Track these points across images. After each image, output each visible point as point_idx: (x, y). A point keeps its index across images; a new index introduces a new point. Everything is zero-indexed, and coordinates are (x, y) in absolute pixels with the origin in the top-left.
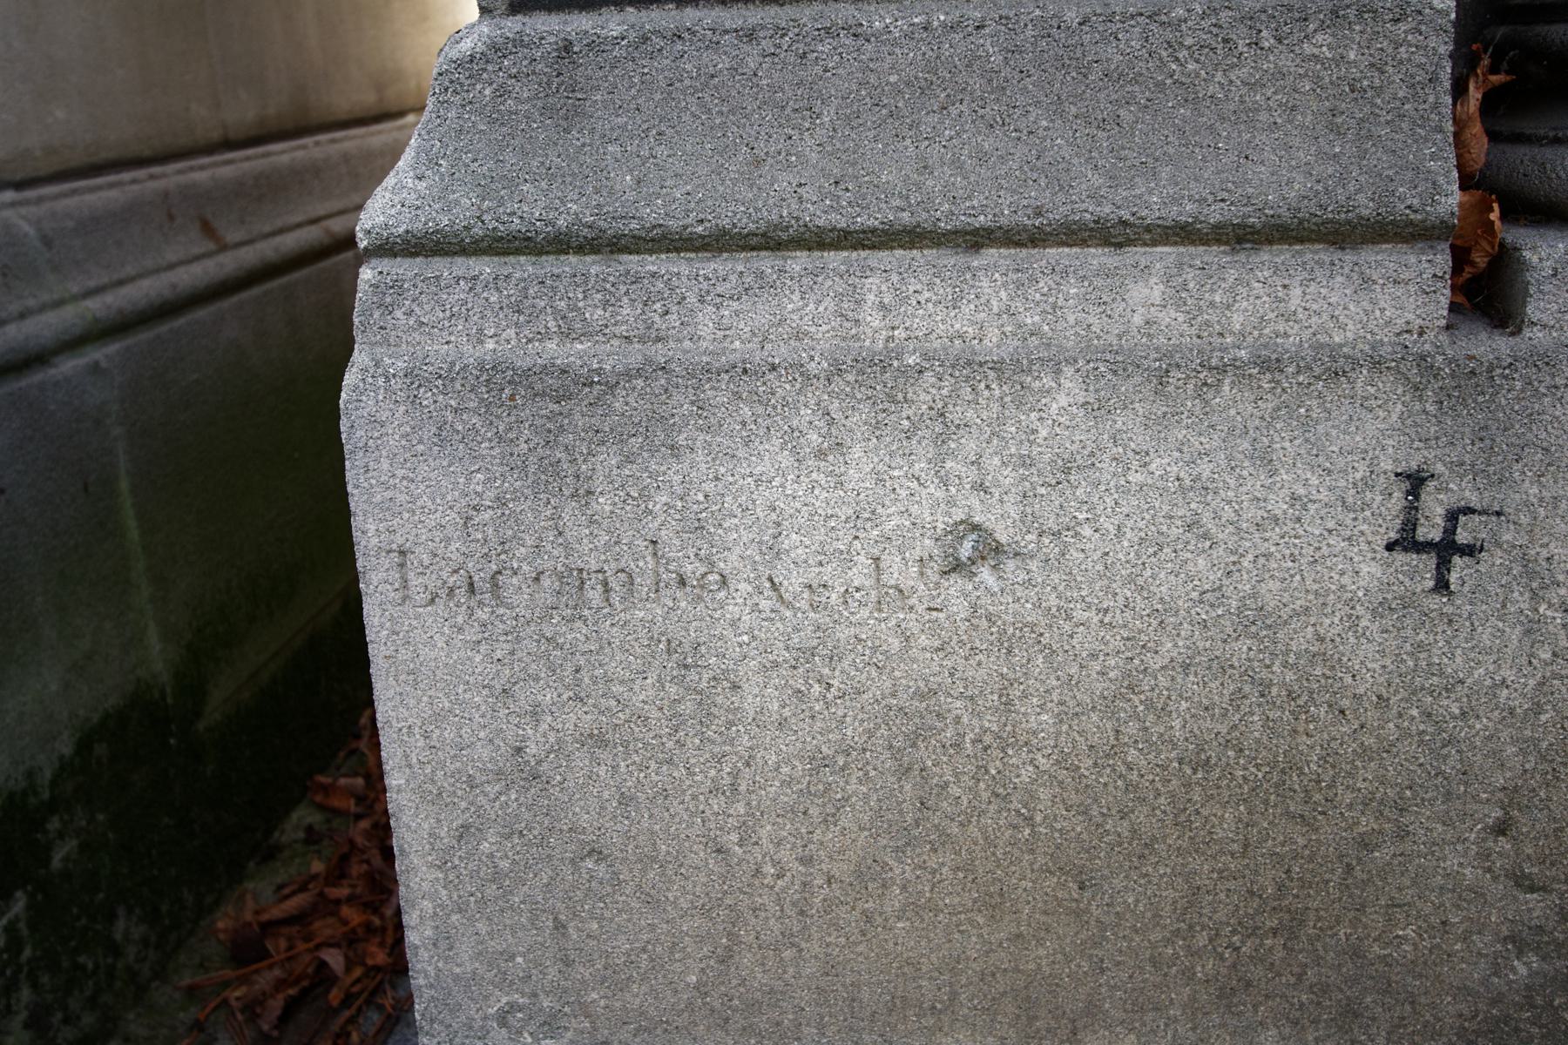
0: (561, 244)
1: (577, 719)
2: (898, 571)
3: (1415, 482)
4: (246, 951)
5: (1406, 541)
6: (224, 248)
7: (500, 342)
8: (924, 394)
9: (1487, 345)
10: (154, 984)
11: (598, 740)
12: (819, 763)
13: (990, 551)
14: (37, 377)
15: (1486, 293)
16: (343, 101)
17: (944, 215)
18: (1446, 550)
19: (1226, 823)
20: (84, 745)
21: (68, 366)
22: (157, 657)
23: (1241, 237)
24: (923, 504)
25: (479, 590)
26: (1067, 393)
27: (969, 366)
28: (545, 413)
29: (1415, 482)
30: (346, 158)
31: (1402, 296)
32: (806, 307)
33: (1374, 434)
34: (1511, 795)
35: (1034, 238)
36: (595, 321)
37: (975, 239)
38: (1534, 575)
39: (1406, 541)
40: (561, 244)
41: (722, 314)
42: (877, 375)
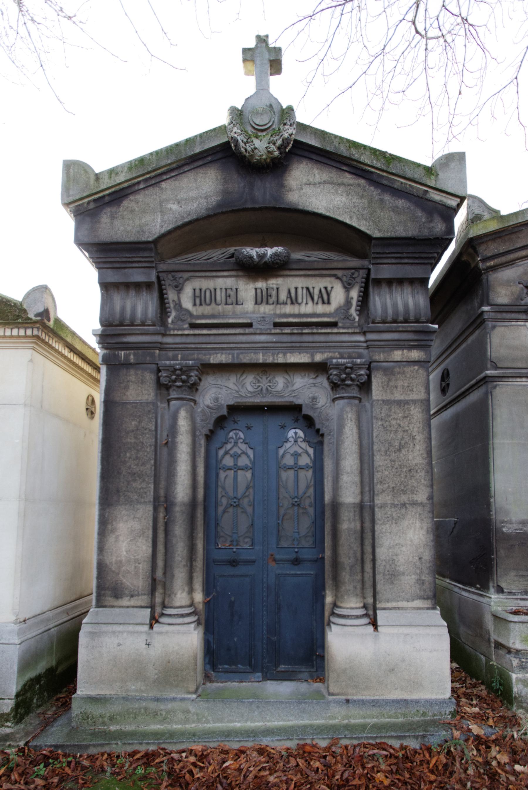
0: (95, 623)
1: (92, 657)
2: (115, 646)
3: (147, 640)
4: (57, 700)
5: (146, 644)
6: (69, 615)
7: (91, 630)
8: (117, 634)
9: (151, 631)
10: (137, 520)
11: (93, 659)
12: (109, 660)
13: (121, 645)
14: (50, 631)
15: (151, 627)
16: (86, 594)
17: (119, 622)
18: (149, 645)
19: (136, 665)
20: (46, 671)
21: (52, 630)
22: (54, 663)
23: (137, 624)
24: (116, 641)
25: (87, 647)
26: (125, 634)
27: (119, 632)
28: (93, 635)
29: (147, 640)
30: (86, 602)
31: (146, 628)
32: (110, 628)
33: (144, 637)
34: (154, 663)
35: (124, 624)
36: (97, 628)
37: (121, 624)
38: (154, 647)
39: (146, 644)
40: (95, 623)
41: (104, 628)
42: (114, 632)
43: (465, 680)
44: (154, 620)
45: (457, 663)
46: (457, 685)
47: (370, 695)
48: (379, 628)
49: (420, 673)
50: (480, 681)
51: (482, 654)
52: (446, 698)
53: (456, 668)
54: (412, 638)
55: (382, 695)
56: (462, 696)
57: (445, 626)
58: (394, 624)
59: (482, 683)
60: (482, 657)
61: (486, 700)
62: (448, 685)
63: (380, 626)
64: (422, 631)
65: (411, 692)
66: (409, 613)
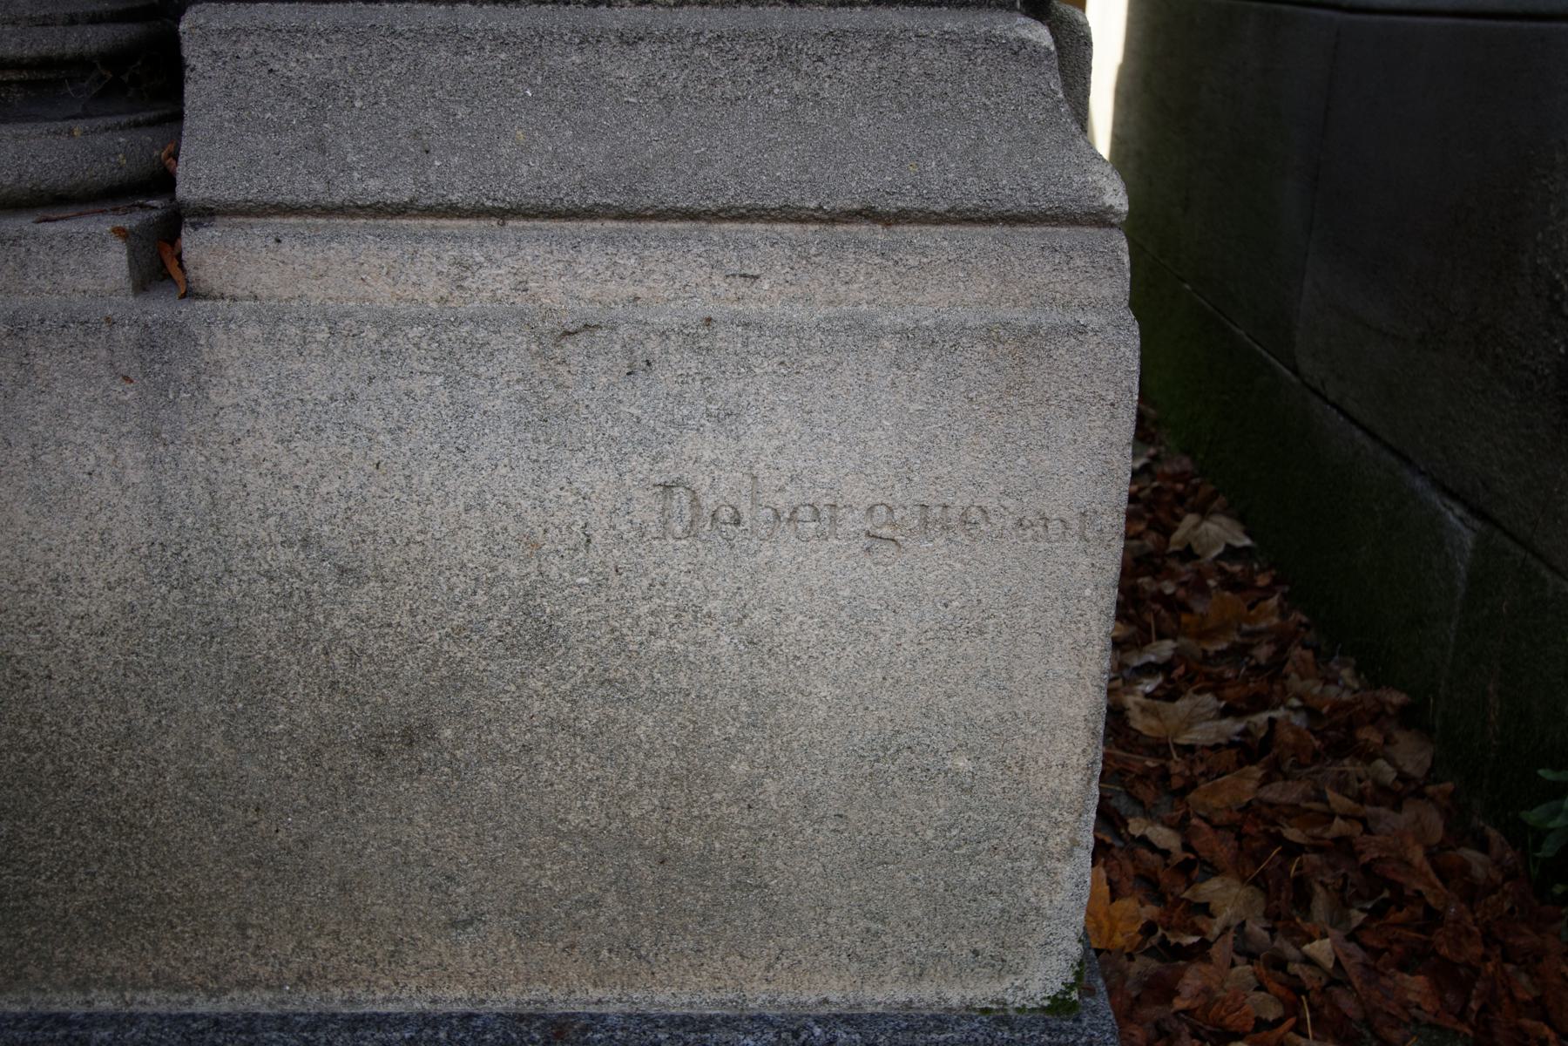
43: (1275, 669)
44: (158, 264)
45: (1243, 519)
46: (1200, 722)
47: (162, 981)
48: (196, 245)
49: (740, 768)
50: (1397, 698)
51: (1453, 496)
52: (1015, 1000)
53: (1231, 552)
54: (639, 368)
55: (305, 978)
56: (1223, 849)
57: (1100, 218)
58: (403, 188)
59: (1409, 717)
60: (1453, 514)
61: (1433, 918)
62: (1064, 890)
63: (207, 213)
64: (781, 281)
65: (630, 947)
66: (630, 40)
